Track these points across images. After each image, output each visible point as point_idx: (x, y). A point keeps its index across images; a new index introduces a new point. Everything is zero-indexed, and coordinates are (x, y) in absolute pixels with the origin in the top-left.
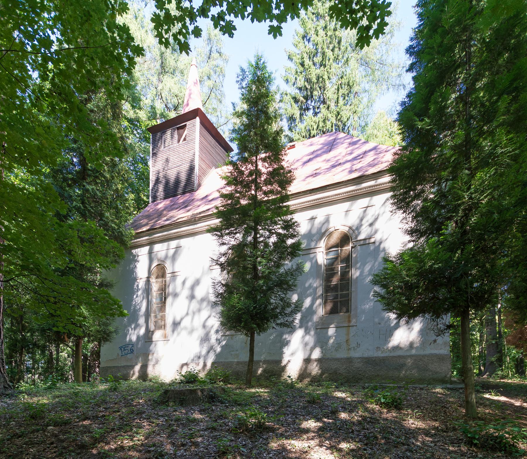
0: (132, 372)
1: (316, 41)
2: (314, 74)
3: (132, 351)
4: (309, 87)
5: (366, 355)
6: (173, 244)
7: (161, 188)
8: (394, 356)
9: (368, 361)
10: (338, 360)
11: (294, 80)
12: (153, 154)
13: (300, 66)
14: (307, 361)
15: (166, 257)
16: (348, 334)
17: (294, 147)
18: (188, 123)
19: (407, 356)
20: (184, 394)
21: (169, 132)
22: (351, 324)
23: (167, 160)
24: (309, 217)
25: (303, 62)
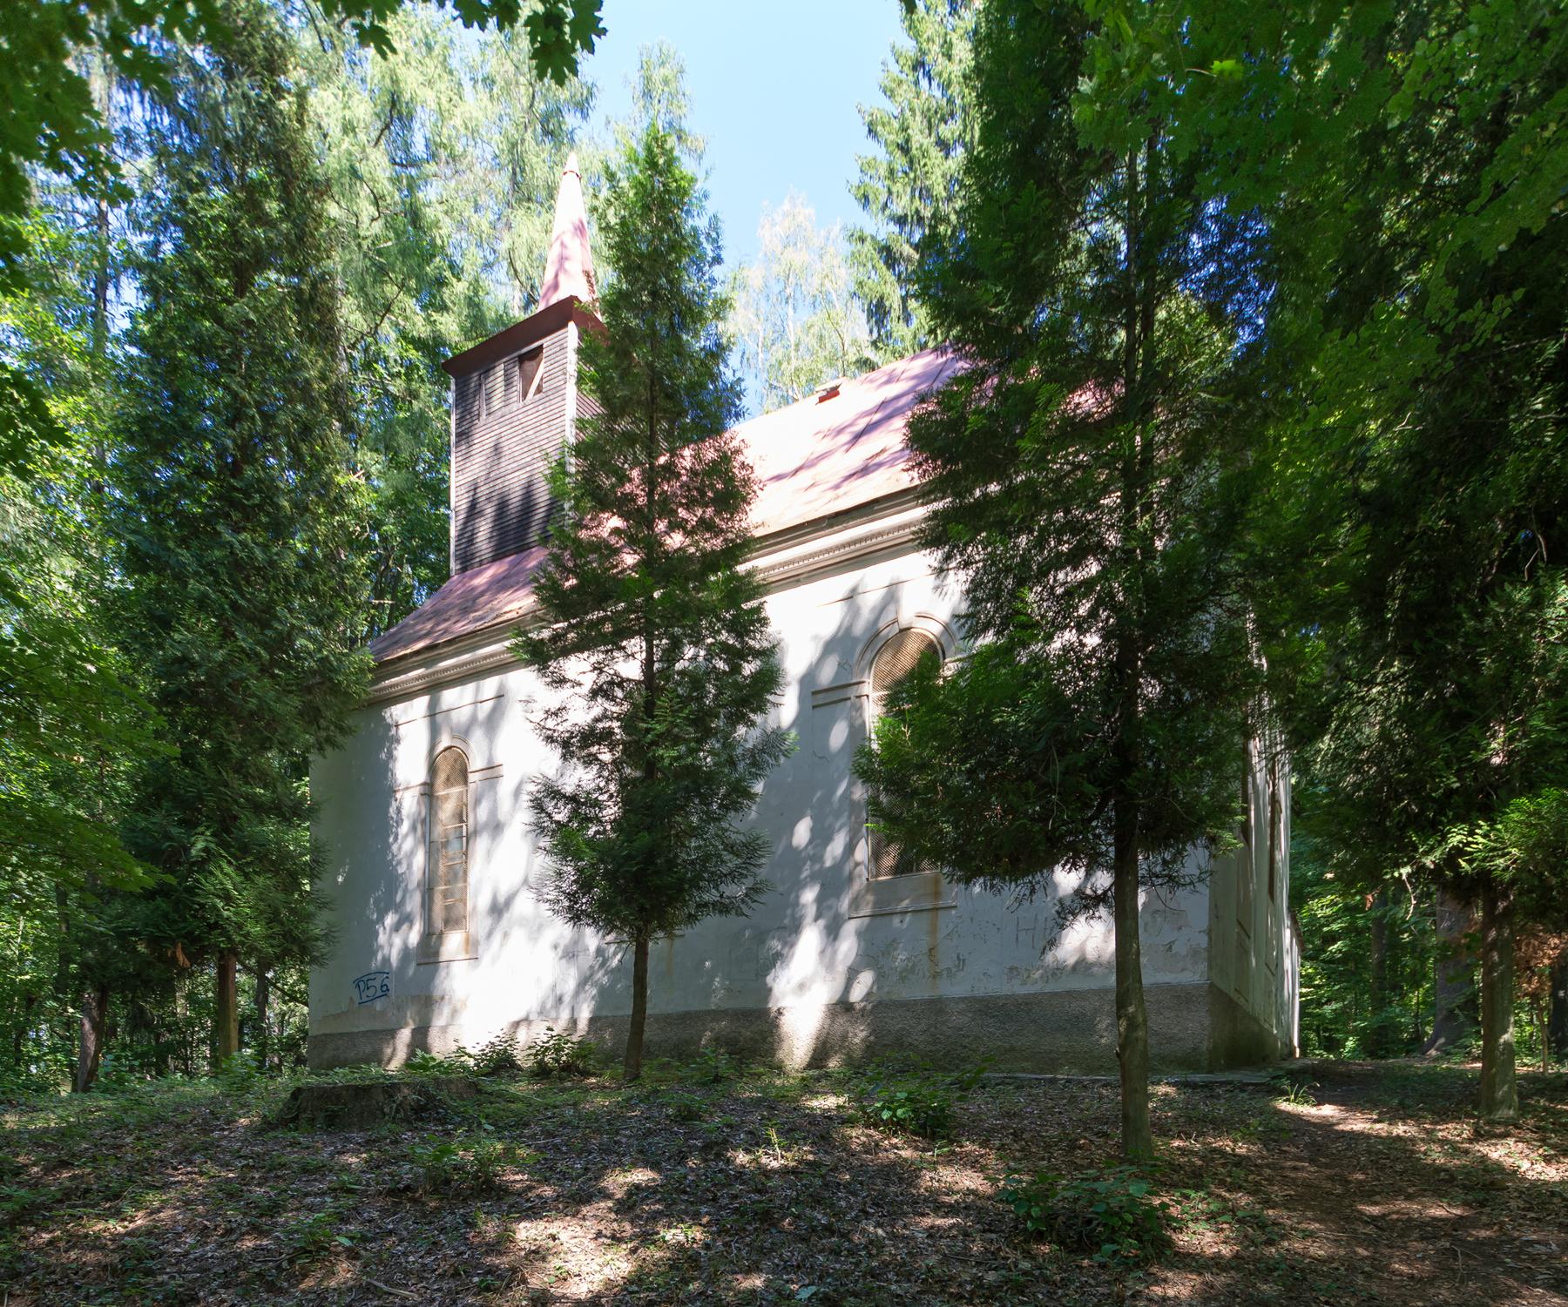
0: (389, 1051)
1: (945, 75)
2: (939, 173)
3: (385, 990)
4: (927, 213)
5: (980, 992)
6: (490, 685)
7: (484, 529)
8: (1056, 994)
9: (985, 1007)
10: (905, 1005)
11: (883, 198)
12: (458, 435)
13: (898, 153)
14: (841, 1007)
15: (473, 720)
16: (934, 931)
17: (837, 394)
18: (546, 342)
19: (1088, 991)
20: (338, 1097)
21: (500, 371)
22: (941, 903)
23: (497, 449)
24: (843, 593)
25: (907, 141)
